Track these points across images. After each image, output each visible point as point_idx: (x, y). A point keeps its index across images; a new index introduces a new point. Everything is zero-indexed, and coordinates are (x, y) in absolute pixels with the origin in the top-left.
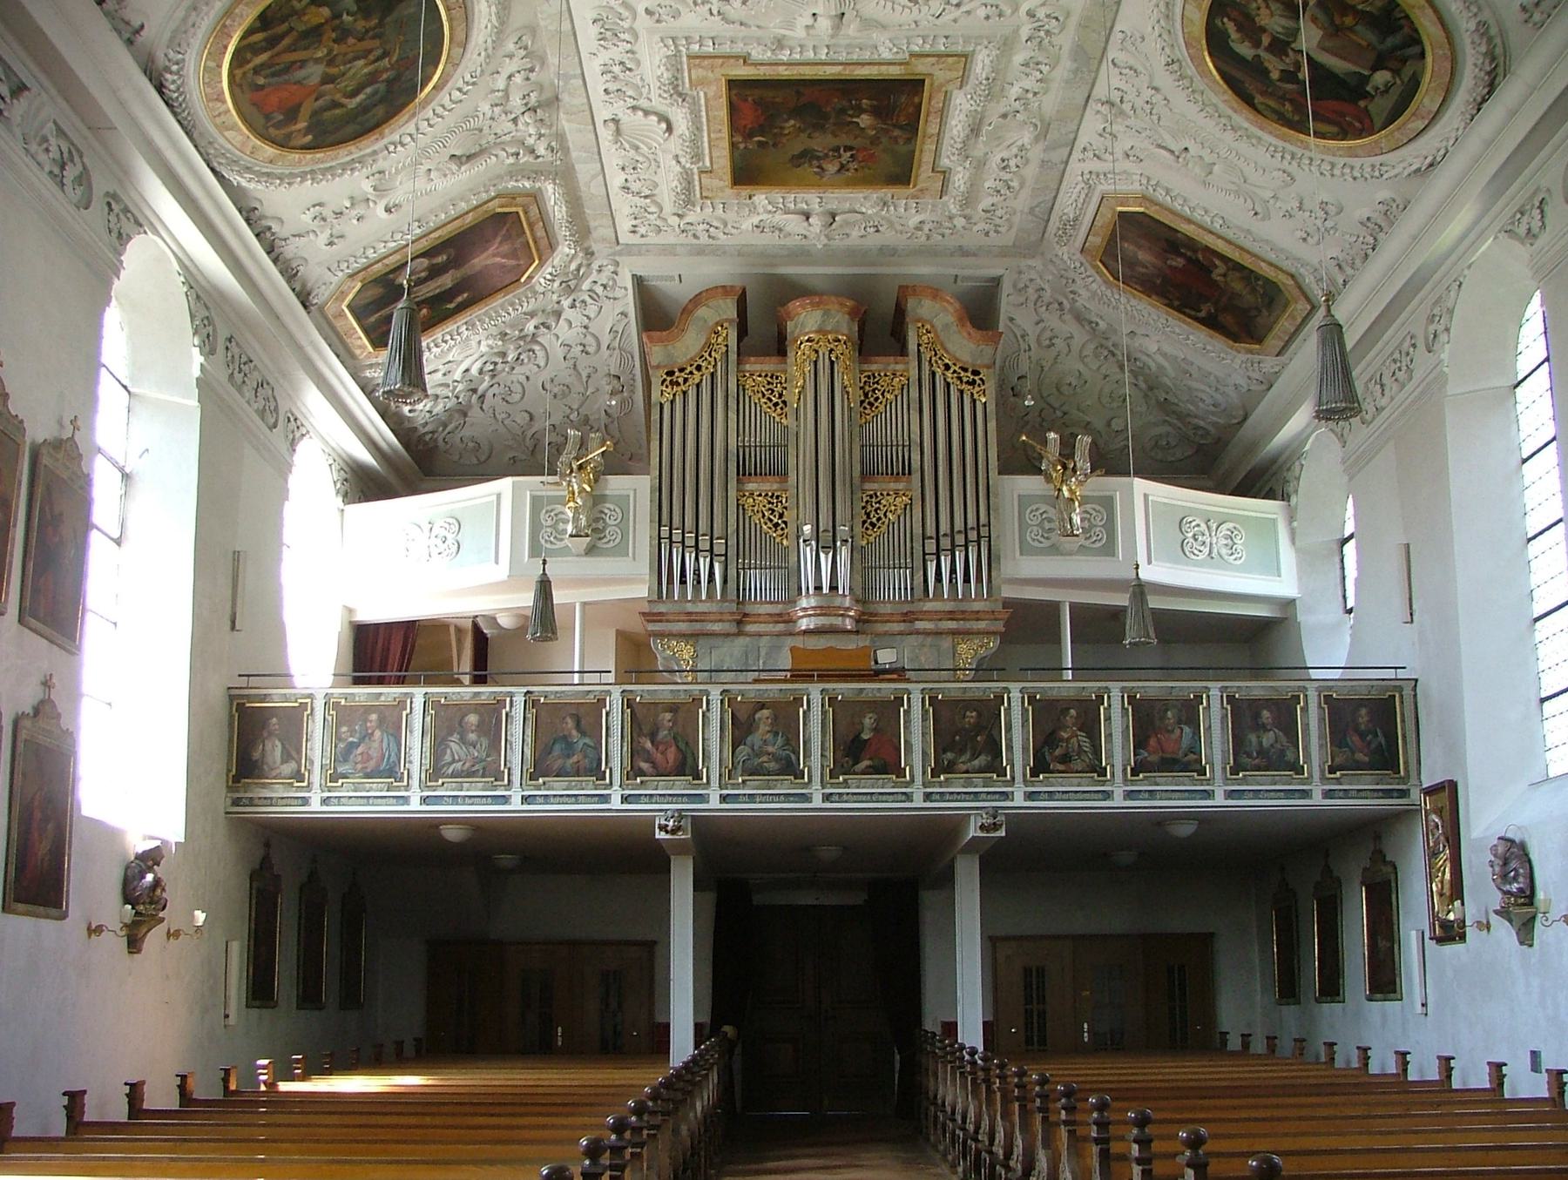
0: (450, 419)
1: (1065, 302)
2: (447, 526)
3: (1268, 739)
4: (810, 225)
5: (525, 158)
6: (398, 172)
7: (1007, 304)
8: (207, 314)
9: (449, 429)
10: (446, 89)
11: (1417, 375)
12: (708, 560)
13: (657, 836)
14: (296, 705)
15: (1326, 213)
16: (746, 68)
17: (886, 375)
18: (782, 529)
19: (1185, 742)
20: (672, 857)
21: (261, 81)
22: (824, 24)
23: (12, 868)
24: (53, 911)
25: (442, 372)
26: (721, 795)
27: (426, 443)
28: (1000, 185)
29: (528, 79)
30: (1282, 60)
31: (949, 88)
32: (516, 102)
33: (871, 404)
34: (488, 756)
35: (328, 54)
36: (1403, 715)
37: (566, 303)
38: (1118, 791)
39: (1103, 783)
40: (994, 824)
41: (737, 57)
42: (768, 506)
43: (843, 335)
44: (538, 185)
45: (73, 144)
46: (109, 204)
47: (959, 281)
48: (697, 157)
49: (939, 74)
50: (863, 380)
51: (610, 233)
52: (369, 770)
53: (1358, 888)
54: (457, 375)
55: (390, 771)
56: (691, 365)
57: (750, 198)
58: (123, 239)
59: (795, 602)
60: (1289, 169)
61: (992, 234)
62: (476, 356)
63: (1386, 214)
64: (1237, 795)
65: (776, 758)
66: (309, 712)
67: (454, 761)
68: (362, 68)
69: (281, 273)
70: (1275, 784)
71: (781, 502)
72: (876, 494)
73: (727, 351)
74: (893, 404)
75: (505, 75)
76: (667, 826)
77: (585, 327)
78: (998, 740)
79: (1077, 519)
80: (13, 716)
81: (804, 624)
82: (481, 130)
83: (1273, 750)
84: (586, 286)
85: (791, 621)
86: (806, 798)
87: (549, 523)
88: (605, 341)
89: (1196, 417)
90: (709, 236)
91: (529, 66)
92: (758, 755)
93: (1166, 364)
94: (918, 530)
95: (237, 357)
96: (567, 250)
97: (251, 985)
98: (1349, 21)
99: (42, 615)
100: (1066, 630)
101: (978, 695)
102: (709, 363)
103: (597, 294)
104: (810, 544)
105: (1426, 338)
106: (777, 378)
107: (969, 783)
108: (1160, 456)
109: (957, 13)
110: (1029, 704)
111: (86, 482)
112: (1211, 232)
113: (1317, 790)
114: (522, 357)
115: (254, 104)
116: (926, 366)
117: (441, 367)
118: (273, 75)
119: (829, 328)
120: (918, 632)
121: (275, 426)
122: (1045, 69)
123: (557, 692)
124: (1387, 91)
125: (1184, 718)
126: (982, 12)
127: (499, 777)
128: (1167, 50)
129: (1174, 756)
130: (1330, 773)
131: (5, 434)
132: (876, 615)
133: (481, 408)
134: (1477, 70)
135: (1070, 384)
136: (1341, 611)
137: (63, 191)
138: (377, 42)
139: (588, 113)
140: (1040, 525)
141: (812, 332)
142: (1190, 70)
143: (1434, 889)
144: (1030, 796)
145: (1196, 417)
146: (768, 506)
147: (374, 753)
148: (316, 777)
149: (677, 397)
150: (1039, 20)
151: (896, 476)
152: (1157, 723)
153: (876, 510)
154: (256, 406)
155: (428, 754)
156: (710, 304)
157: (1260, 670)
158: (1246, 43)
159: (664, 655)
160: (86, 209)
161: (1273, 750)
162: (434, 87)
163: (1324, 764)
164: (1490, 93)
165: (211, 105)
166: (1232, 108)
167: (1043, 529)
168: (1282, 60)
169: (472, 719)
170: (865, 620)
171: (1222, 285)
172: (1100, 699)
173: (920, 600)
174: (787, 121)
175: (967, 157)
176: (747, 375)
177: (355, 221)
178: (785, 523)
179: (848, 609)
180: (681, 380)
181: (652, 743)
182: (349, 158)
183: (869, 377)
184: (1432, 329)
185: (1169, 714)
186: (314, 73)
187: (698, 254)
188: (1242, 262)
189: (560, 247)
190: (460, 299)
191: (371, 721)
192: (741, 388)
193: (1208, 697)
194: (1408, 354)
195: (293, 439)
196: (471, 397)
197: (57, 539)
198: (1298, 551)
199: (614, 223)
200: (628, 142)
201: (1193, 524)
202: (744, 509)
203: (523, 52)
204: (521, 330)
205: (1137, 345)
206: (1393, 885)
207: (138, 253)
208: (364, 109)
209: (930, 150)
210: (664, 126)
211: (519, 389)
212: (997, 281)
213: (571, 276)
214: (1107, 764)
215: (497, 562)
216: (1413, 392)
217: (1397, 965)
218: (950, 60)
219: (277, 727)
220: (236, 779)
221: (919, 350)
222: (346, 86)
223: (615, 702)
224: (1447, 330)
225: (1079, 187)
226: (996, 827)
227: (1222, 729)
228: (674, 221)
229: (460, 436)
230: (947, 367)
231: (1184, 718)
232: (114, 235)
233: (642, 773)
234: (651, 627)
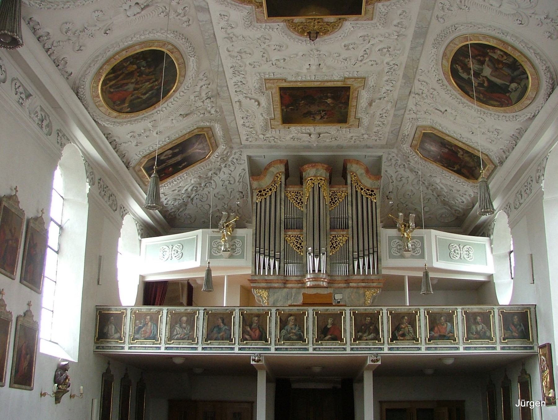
0: (181, 207)
1: (406, 164)
2: (178, 247)
3: (479, 328)
4: (311, 138)
5: (207, 115)
6: (161, 120)
7: (384, 166)
8: (92, 171)
9: (180, 211)
10: (178, 92)
11: (533, 192)
12: (273, 260)
13: (251, 363)
14: (120, 312)
15: (498, 133)
16: (285, 83)
17: (339, 192)
18: (301, 249)
19: (449, 328)
20: (258, 370)
21: (112, 90)
22: (313, 68)
23: (14, 371)
24: (28, 387)
25: (177, 190)
26: (275, 348)
27: (172, 216)
28: (379, 123)
29: (207, 87)
30: (478, 79)
31: (360, 89)
32: (204, 95)
33: (334, 203)
34: (190, 332)
35: (136, 81)
36: (531, 318)
37: (223, 165)
38: (423, 347)
39: (417, 344)
40: (377, 359)
41: (282, 80)
42: (295, 240)
43: (323, 178)
44: (212, 124)
45: (46, 113)
46: (58, 133)
47: (366, 157)
48: (268, 114)
49: (355, 85)
50: (331, 194)
51: (238, 141)
52: (146, 337)
53: (517, 384)
54: (183, 192)
55: (154, 337)
56: (268, 189)
57: (289, 128)
58: (62, 145)
59: (305, 276)
60: (483, 117)
61: (378, 140)
62: (190, 185)
63: (519, 133)
64: (467, 349)
65: (295, 334)
66: (125, 315)
67: (177, 334)
68: (147, 85)
69: (119, 156)
70: (482, 345)
71: (300, 239)
72: (335, 236)
73: (281, 183)
74: (342, 203)
75: (199, 86)
76: (255, 359)
77: (230, 174)
78: (378, 328)
79: (410, 245)
80: (16, 316)
81: (308, 284)
82: (191, 105)
83: (482, 332)
84: (230, 159)
85: (304, 283)
86: (307, 349)
87: (215, 246)
88: (237, 180)
89: (455, 206)
90: (275, 142)
91: (208, 83)
92: (289, 333)
93: (443, 187)
94: (351, 250)
95: (102, 186)
96: (223, 147)
97: (101, 417)
98: (500, 66)
99: (28, 280)
100: (406, 284)
101: (371, 311)
102: (274, 188)
103: (234, 162)
104: (311, 255)
105: (536, 178)
106: (299, 193)
107: (367, 344)
108: (442, 221)
109: (361, 64)
110: (390, 315)
111: (46, 232)
112: (457, 140)
113: (498, 347)
114: (207, 185)
115: (109, 98)
116: (354, 188)
117: (177, 188)
118: (116, 88)
119: (318, 175)
120: (351, 287)
121: (116, 210)
122: (394, 82)
123: (215, 309)
124: (516, 90)
125: (448, 320)
126: (370, 63)
127: (194, 340)
128: (437, 76)
129: (444, 334)
130: (503, 340)
131: (18, 216)
132: (335, 281)
133: (192, 203)
134: (547, 83)
135: (408, 194)
136: (510, 278)
137: (42, 130)
138: (153, 77)
139: (229, 99)
140: (396, 247)
141: (312, 177)
142: (446, 82)
143: (544, 385)
144: (390, 349)
145: (455, 206)
146: (295, 240)
147: (148, 331)
148: (127, 339)
149: (263, 200)
150: (390, 66)
151: (342, 229)
152: (438, 322)
153: (335, 242)
154: (109, 203)
155: (168, 331)
156: (275, 166)
157: (481, 302)
158: (465, 73)
159: (257, 295)
160: (50, 135)
161: (482, 332)
162: (174, 91)
163: (501, 337)
164: (553, 91)
165: (94, 99)
166: (461, 96)
167: (397, 249)
168: (478, 79)
169: (184, 319)
170: (331, 282)
171: (462, 159)
172: (416, 313)
173: (351, 275)
174: (301, 101)
175: (367, 113)
176: (288, 192)
177: (146, 138)
178: (302, 247)
179: (324, 279)
180: (264, 194)
181: (250, 328)
182: (143, 116)
183: (333, 193)
184: (538, 174)
185: (442, 318)
186: (131, 87)
187: (271, 148)
188: (468, 150)
189: (220, 146)
190: (184, 164)
191: (147, 319)
192: (286, 197)
193: (420, 312)
194: (530, 184)
195: (123, 215)
196: (188, 199)
197: (34, 253)
198: (493, 255)
199: (240, 137)
200: (244, 109)
201: (454, 246)
202: (287, 242)
203: (205, 79)
204: (207, 175)
205: (432, 180)
206: (529, 382)
207: (66, 152)
208: (149, 99)
209: (354, 111)
210: (257, 103)
211: (206, 196)
212: (380, 158)
213: (224, 156)
214: (419, 337)
215: (196, 260)
216: (533, 196)
217: (532, 414)
218: (359, 80)
219: (113, 320)
220: (98, 339)
221: (351, 183)
222: (142, 91)
223: (237, 314)
224: (543, 175)
225: (408, 124)
226: (377, 361)
227: (462, 323)
228: (261, 136)
229: (184, 213)
230: (362, 189)
231: (448, 320)
232: (59, 144)
233: (246, 340)
234: (252, 285)
